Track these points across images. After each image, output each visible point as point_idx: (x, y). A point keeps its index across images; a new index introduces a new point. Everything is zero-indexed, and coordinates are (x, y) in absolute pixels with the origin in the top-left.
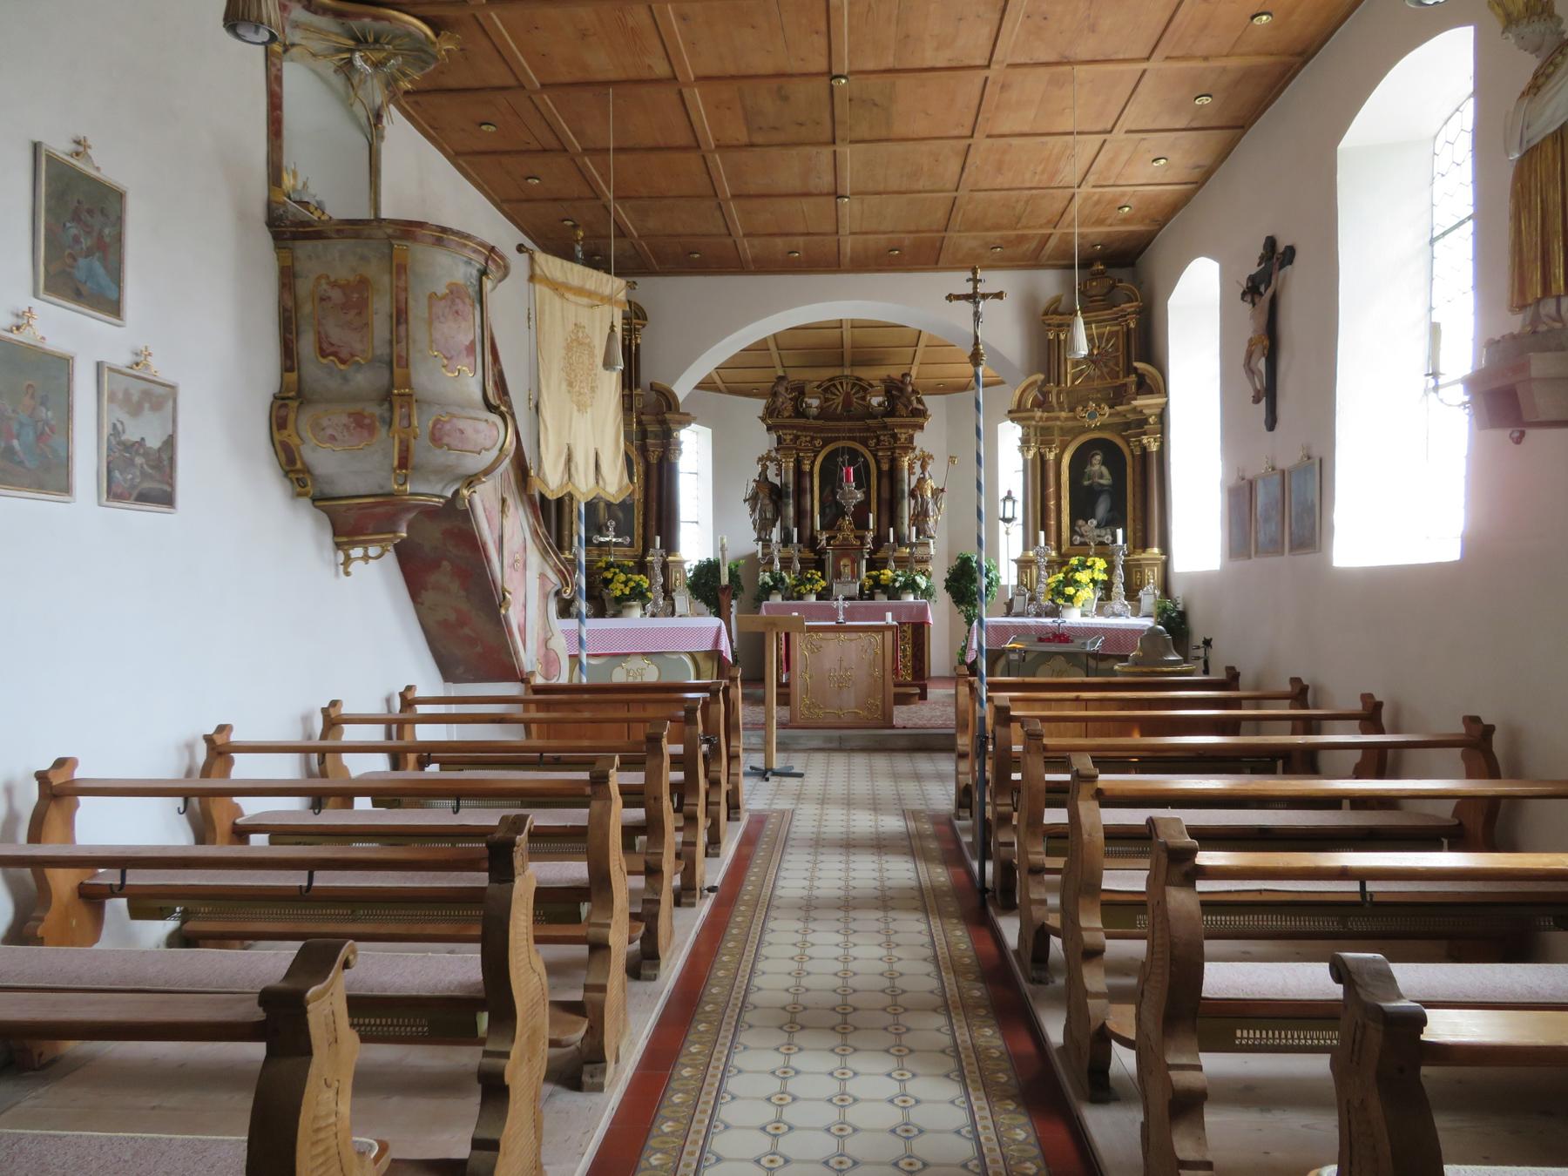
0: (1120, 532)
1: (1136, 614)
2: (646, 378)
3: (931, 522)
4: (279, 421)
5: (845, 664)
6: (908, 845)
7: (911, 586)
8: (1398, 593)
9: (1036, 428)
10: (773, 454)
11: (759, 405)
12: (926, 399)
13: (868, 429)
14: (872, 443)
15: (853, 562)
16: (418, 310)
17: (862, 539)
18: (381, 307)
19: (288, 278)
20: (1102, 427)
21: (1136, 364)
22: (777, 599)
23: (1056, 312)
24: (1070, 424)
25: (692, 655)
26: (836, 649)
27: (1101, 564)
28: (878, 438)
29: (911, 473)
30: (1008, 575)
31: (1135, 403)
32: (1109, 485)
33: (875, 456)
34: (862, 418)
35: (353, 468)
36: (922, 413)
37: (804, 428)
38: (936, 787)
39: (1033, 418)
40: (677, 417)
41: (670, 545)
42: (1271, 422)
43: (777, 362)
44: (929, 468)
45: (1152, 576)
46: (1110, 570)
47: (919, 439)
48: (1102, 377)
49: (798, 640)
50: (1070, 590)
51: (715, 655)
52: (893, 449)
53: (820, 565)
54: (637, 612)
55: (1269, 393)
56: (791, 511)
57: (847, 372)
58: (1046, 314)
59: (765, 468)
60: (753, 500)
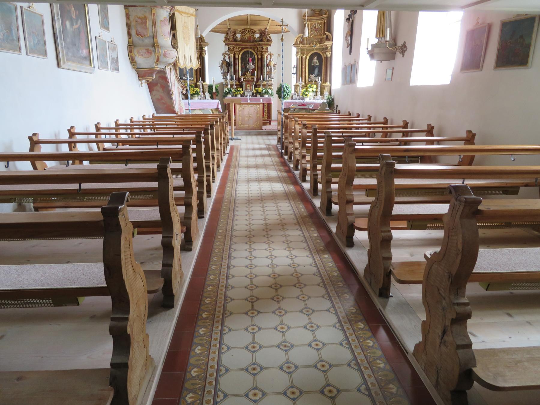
0: (320, 78)
1: (322, 100)
3: (273, 74)
4: (130, 51)
6: (268, 149)
7: (267, 92)
8: (366, 92)
11: (222, 36)
12: (271, 35)
13: (255, 45)
14: (256, 49)
16: (158, 24)
17: (253, 79)
18: (149, 24)
19: (128, 16)
20: (317, 49)
22: (229, 96)
25: (211, 109)
26: (247, 110)
27: (315, 86)
29: (267, 59)
30: (292, 90)
32: (317, 65)
34: (253, 42)
35: (144, 62)
36: (270, 41)
37: (236, 45)
38: (273, 141)
41: (204, 80)
42: (350, 53)
43: (228, 24)
44: (272, 58)
46: (317, 88)
48: (317, 35)
49: (237, 106)
50: (307, 93)
51: (217, 109)
52: (262, 52)
53: (241, 86)
54: (197, 98)
55: (350, 45)
56: (233, 70)
57: (248, 27)
60: (221, 66)
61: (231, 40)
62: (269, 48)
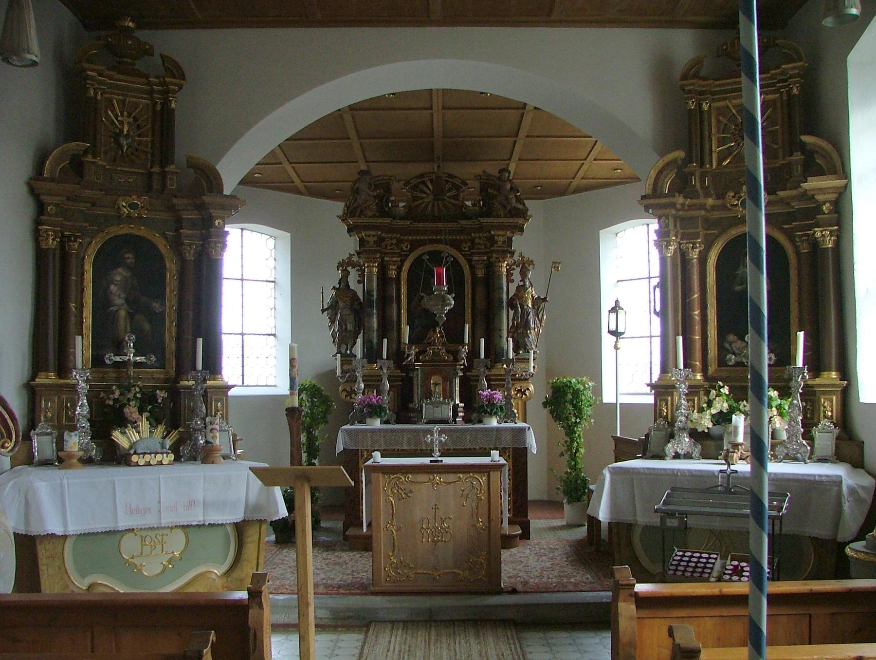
2: (181, 152)
3: (532, 335)
5: (441, 513)
9: (675, 218)
10: (355, 259)
11: (339, 207)
14: (466, 247)
15: (445, 381)
21: (805, 138)
23: (696, 76)
24: (716, 215)
26: (427, 498)
28: (472, 241)
31: (804, 185)
33: (469, 261)
34: (454, 219)
36: (523, 214)
37: (390, 229)
39: (673, 205)
40: (219, 200)
43: (359, 154)
45: (830, 406)
47: (519, 243)
52: (489, 254)
58: (685, 77)
59: (346, 274)
60: (332, 309)
61: (370, 211)
62: (516, 239)
